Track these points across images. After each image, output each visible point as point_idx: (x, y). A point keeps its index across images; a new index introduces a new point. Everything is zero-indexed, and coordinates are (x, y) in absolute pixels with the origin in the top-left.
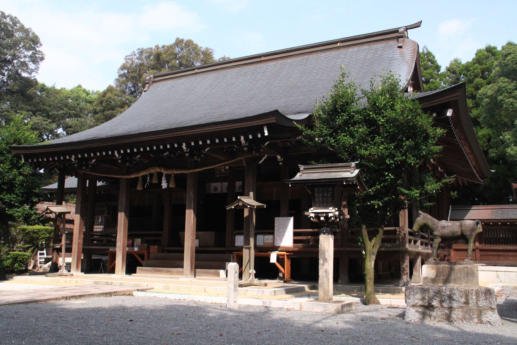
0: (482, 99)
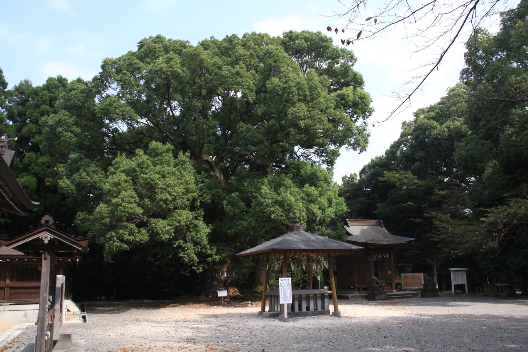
0: (44, 127)
